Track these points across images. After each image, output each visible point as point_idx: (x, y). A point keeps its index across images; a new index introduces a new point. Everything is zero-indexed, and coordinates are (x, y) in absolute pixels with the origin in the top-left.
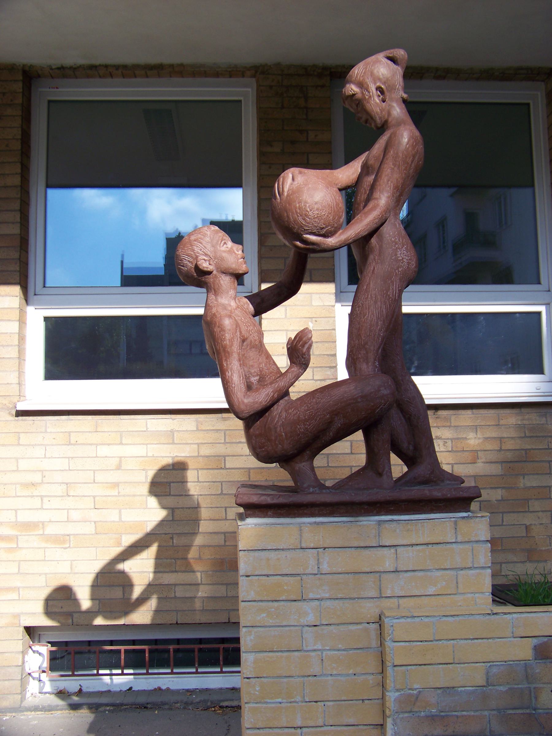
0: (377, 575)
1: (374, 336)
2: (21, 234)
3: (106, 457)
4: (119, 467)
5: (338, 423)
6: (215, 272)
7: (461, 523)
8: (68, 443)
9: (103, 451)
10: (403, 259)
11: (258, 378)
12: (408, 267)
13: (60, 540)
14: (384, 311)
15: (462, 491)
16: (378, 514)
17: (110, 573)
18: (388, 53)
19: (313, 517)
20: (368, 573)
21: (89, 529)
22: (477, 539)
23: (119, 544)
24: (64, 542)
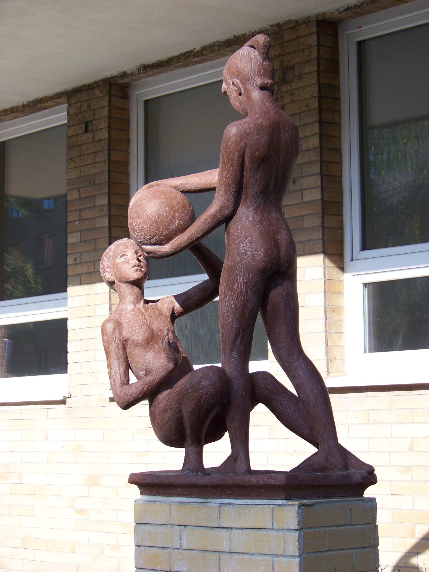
0: (217, 554)
1: (227, 328)
2: (322, 199)
3: (400, 437)
6: (116, 282)
7: (277, 509)
8: (367, 422)
10: (246, 251)
11: (144, 372)
12: (253, 259)
14: (232, 303)
15: (271, 479)
16: (220, 497)
17: (405, 567)
19: (179, 497)
20: (213, 551)
22: (288, 527)
23: (413, 535)
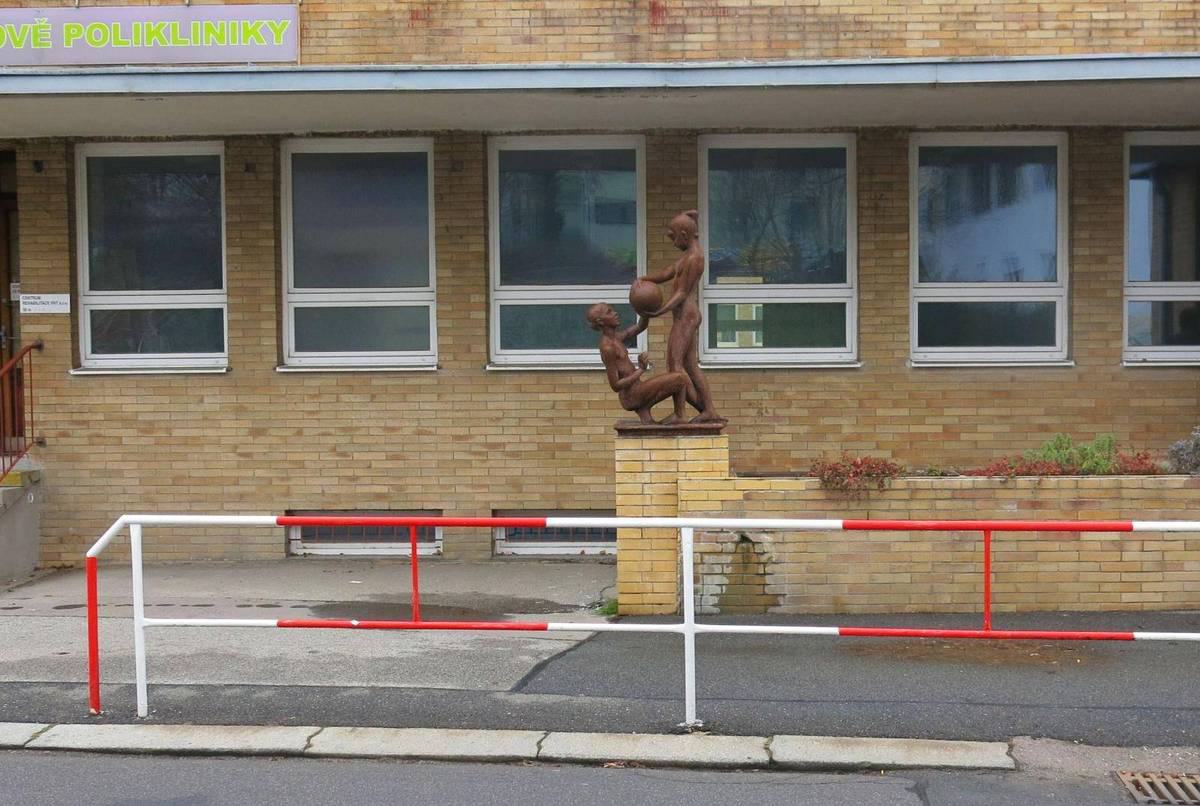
4: (553, 408)
5: (660, 394)
9: (543, 397)
13: (515, 455)
18: (689, 212)
21: (534, 447)
24: (517, 456)
